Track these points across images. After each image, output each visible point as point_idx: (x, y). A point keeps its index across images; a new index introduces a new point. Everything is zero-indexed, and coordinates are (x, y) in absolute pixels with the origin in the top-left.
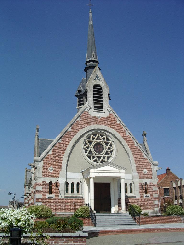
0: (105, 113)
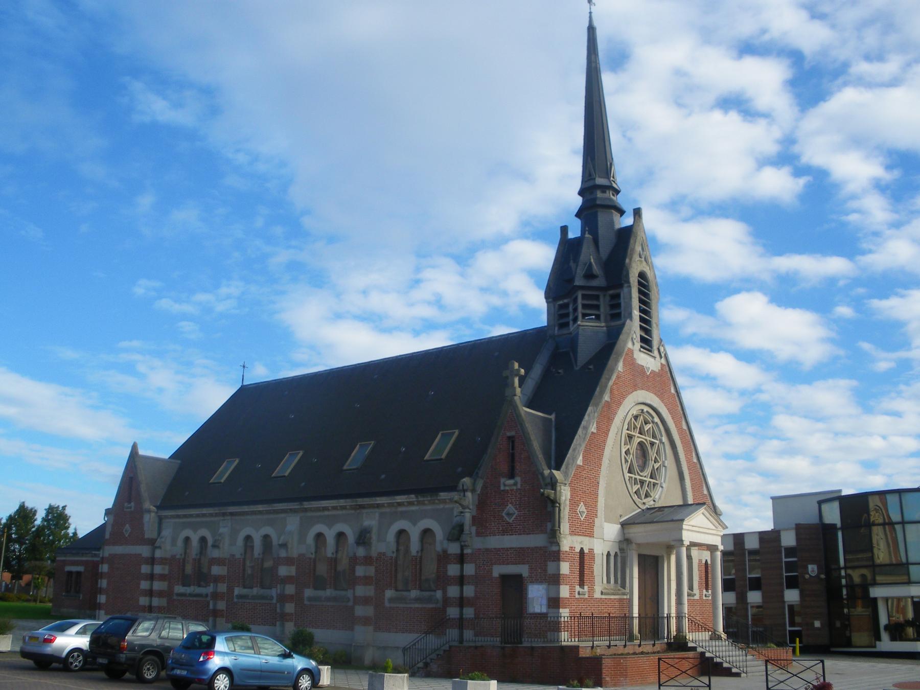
0: (655, 357)
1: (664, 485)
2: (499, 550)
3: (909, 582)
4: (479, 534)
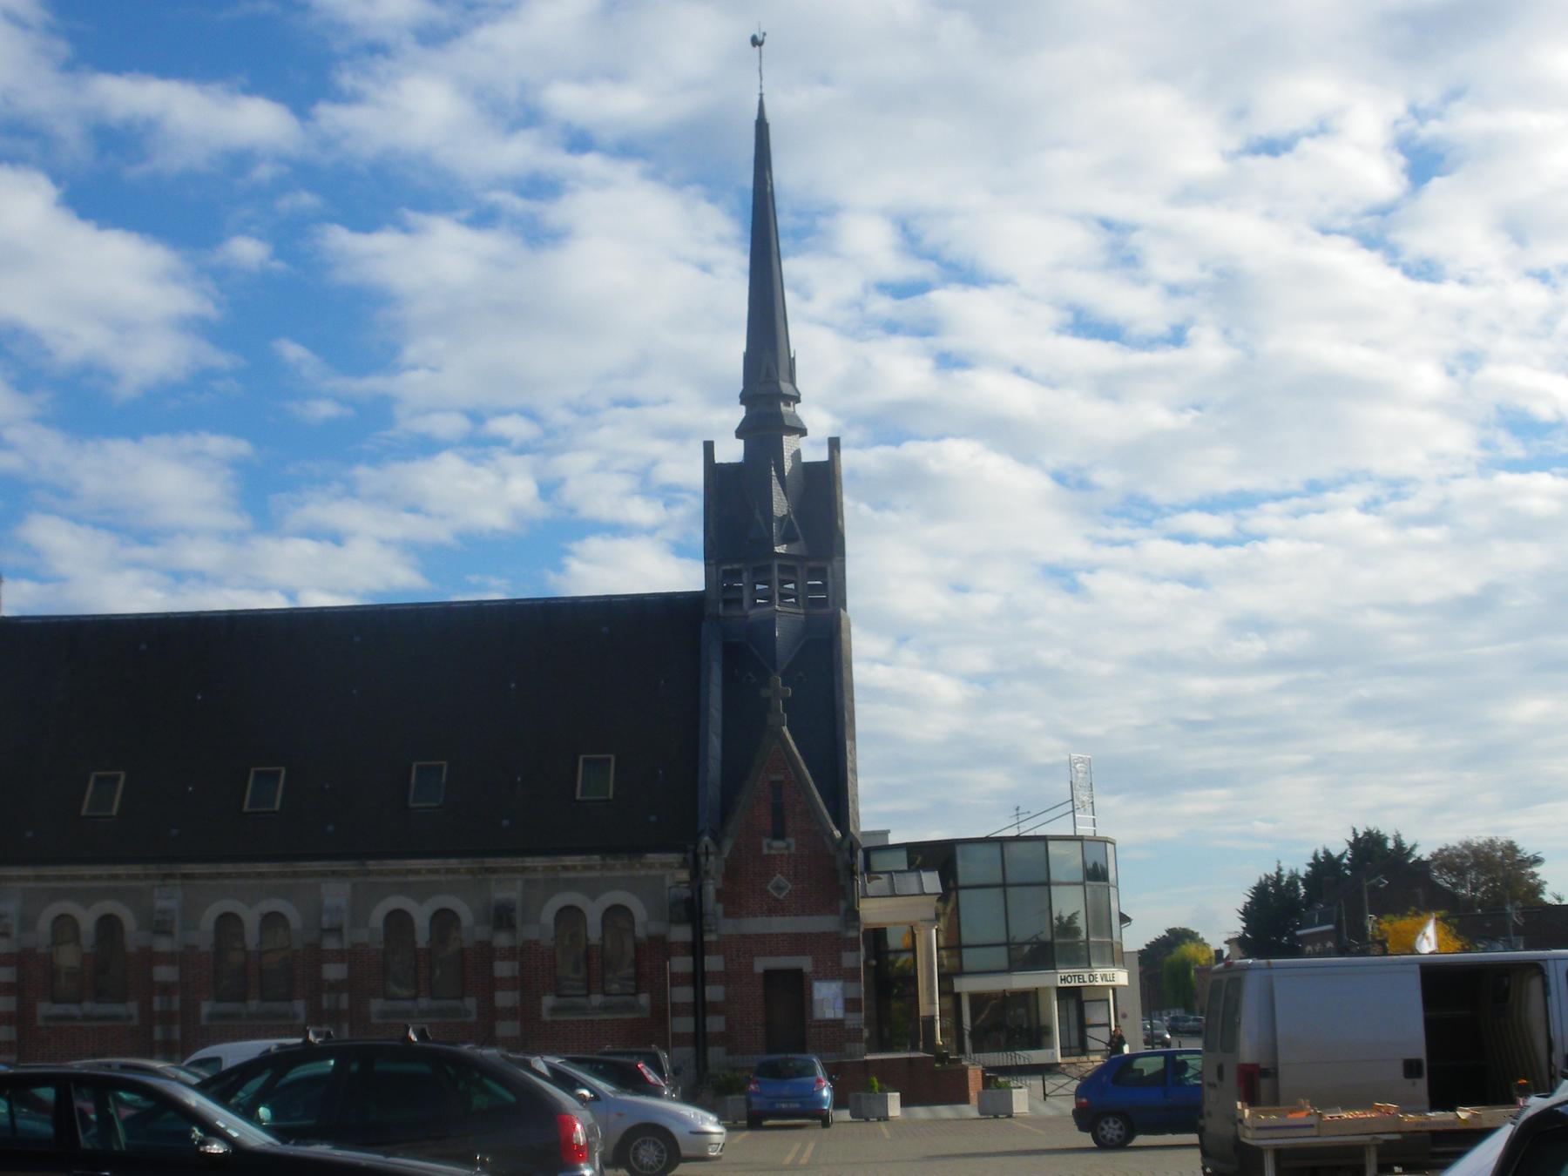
2: (764, 936)
4: (726, 914)
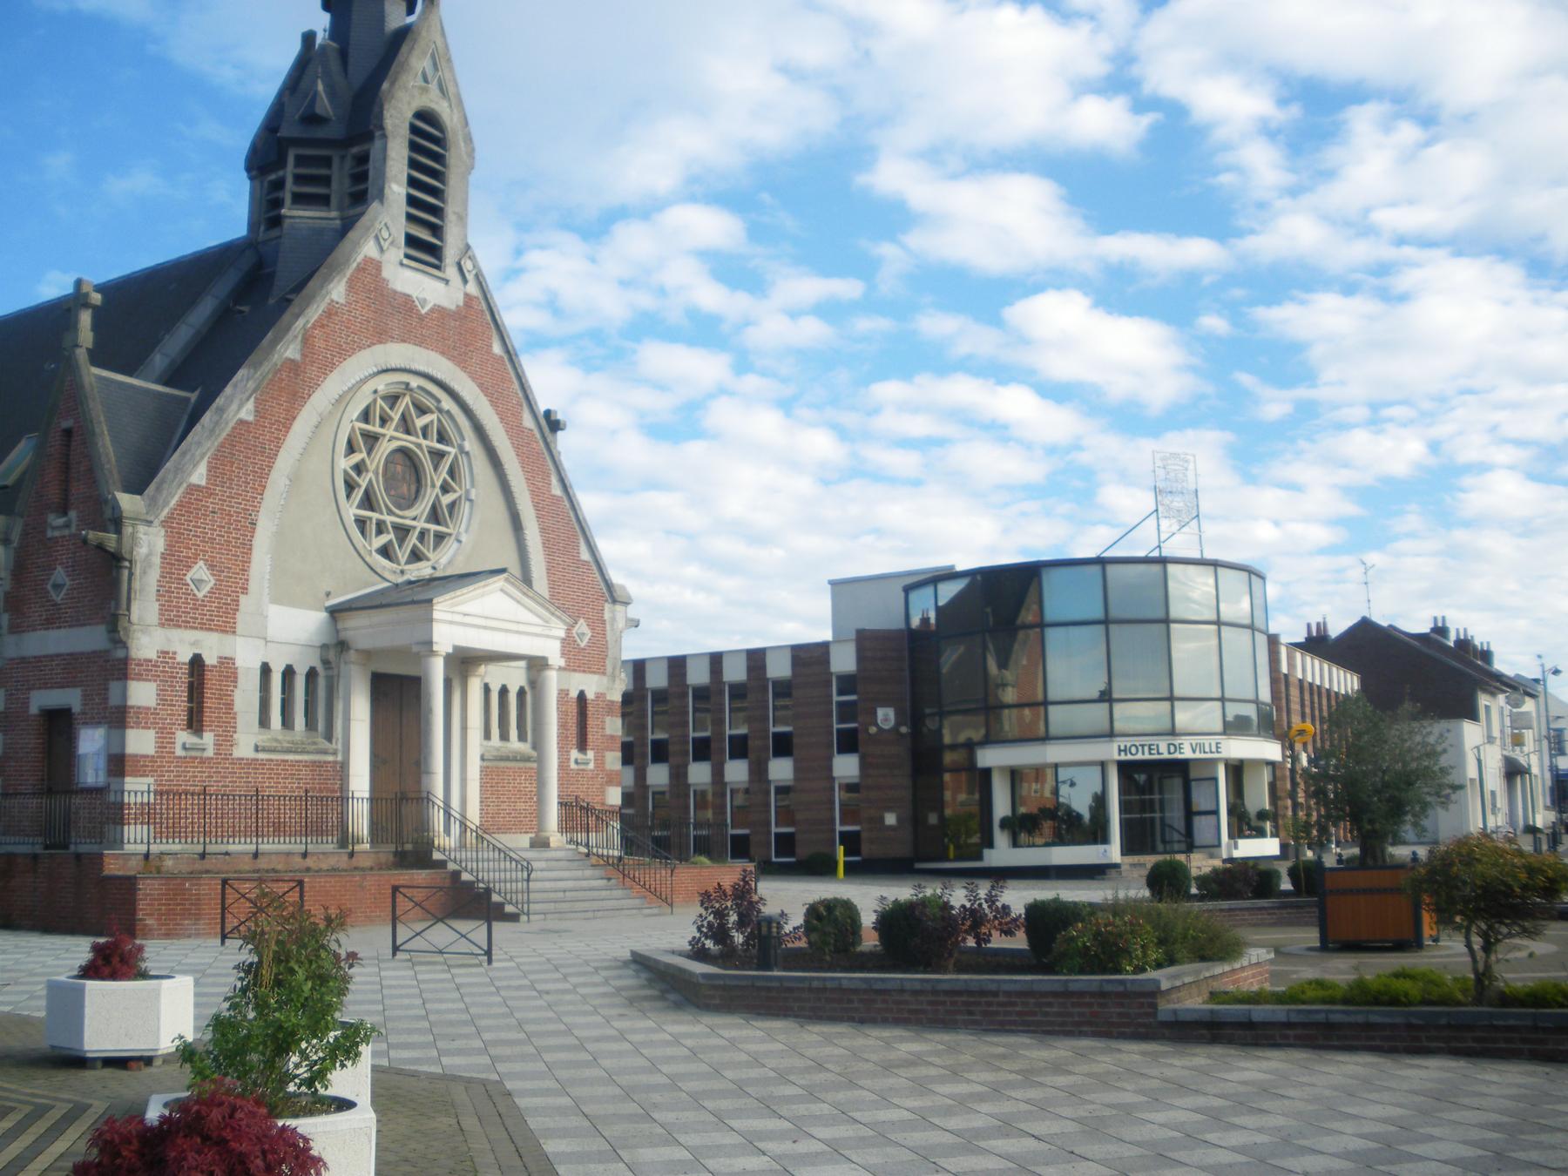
0: (447, 282)
1: (464, 538)
3: (1046, 738)
